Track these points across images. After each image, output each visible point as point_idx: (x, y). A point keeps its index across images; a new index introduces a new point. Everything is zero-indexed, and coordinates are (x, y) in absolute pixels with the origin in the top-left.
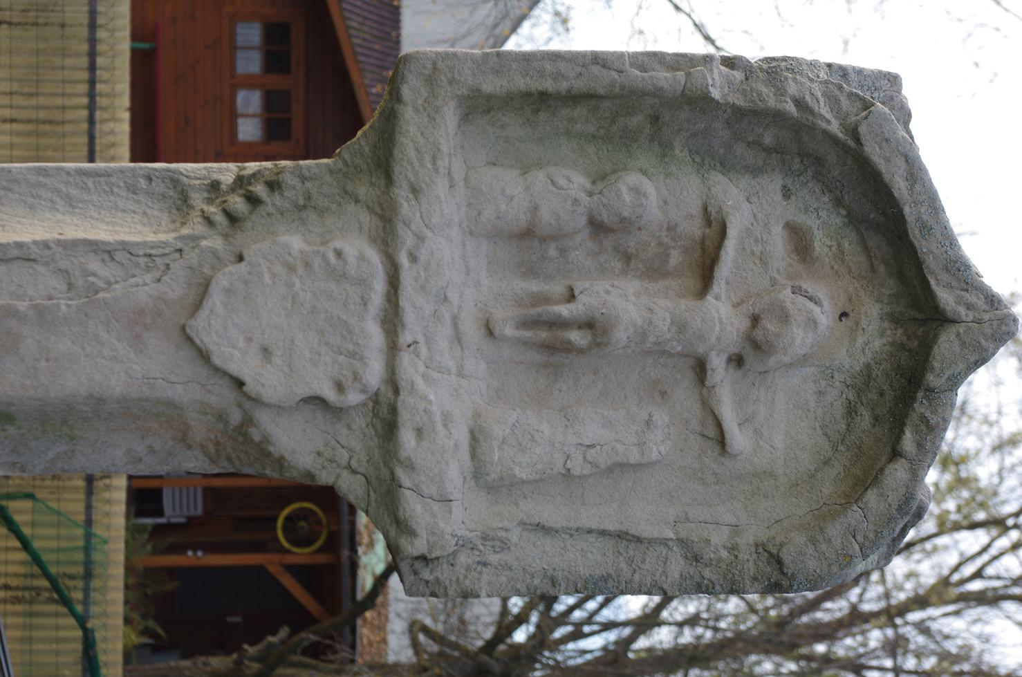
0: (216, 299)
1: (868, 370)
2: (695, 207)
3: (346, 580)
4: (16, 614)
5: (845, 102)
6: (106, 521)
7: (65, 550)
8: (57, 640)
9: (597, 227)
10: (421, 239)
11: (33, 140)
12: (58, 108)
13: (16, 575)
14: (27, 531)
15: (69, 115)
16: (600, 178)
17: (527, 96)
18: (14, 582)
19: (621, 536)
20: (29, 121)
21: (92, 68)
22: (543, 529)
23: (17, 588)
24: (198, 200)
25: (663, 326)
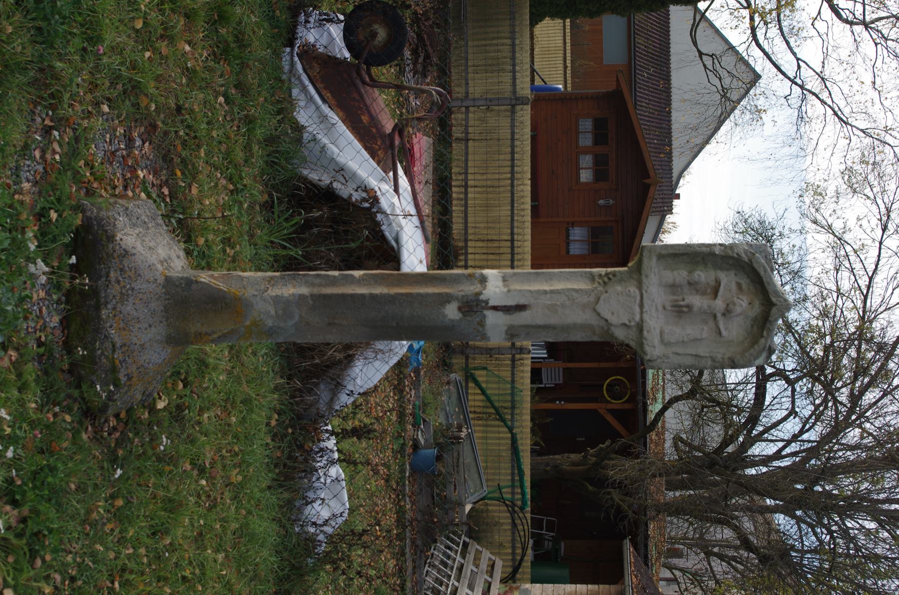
0: (601, 302)
1: (756, 317)
2: (713, 278)
3: (641, 417)
4: (479, 425)
5: (749, 254)
6: (521, 381)
7: (502, 395)
8: (499, 438)
9: (690, 283)
10: (648, 287)
11: (485, 195)
12: (496, 179)
13: (479, 406)
14: (484, 385)
15: (502, 183)
16: (690, 272)
17: (672, 254)
18: (478, 410)
19: (696, 356)
20: (483, 187)
21: (513, 159)
22: (677, 354)
23: (480, 413)
24: (597, 278)
25: (705, 306)
